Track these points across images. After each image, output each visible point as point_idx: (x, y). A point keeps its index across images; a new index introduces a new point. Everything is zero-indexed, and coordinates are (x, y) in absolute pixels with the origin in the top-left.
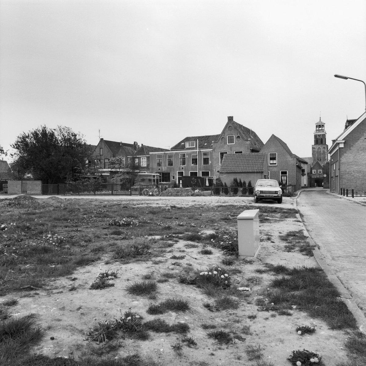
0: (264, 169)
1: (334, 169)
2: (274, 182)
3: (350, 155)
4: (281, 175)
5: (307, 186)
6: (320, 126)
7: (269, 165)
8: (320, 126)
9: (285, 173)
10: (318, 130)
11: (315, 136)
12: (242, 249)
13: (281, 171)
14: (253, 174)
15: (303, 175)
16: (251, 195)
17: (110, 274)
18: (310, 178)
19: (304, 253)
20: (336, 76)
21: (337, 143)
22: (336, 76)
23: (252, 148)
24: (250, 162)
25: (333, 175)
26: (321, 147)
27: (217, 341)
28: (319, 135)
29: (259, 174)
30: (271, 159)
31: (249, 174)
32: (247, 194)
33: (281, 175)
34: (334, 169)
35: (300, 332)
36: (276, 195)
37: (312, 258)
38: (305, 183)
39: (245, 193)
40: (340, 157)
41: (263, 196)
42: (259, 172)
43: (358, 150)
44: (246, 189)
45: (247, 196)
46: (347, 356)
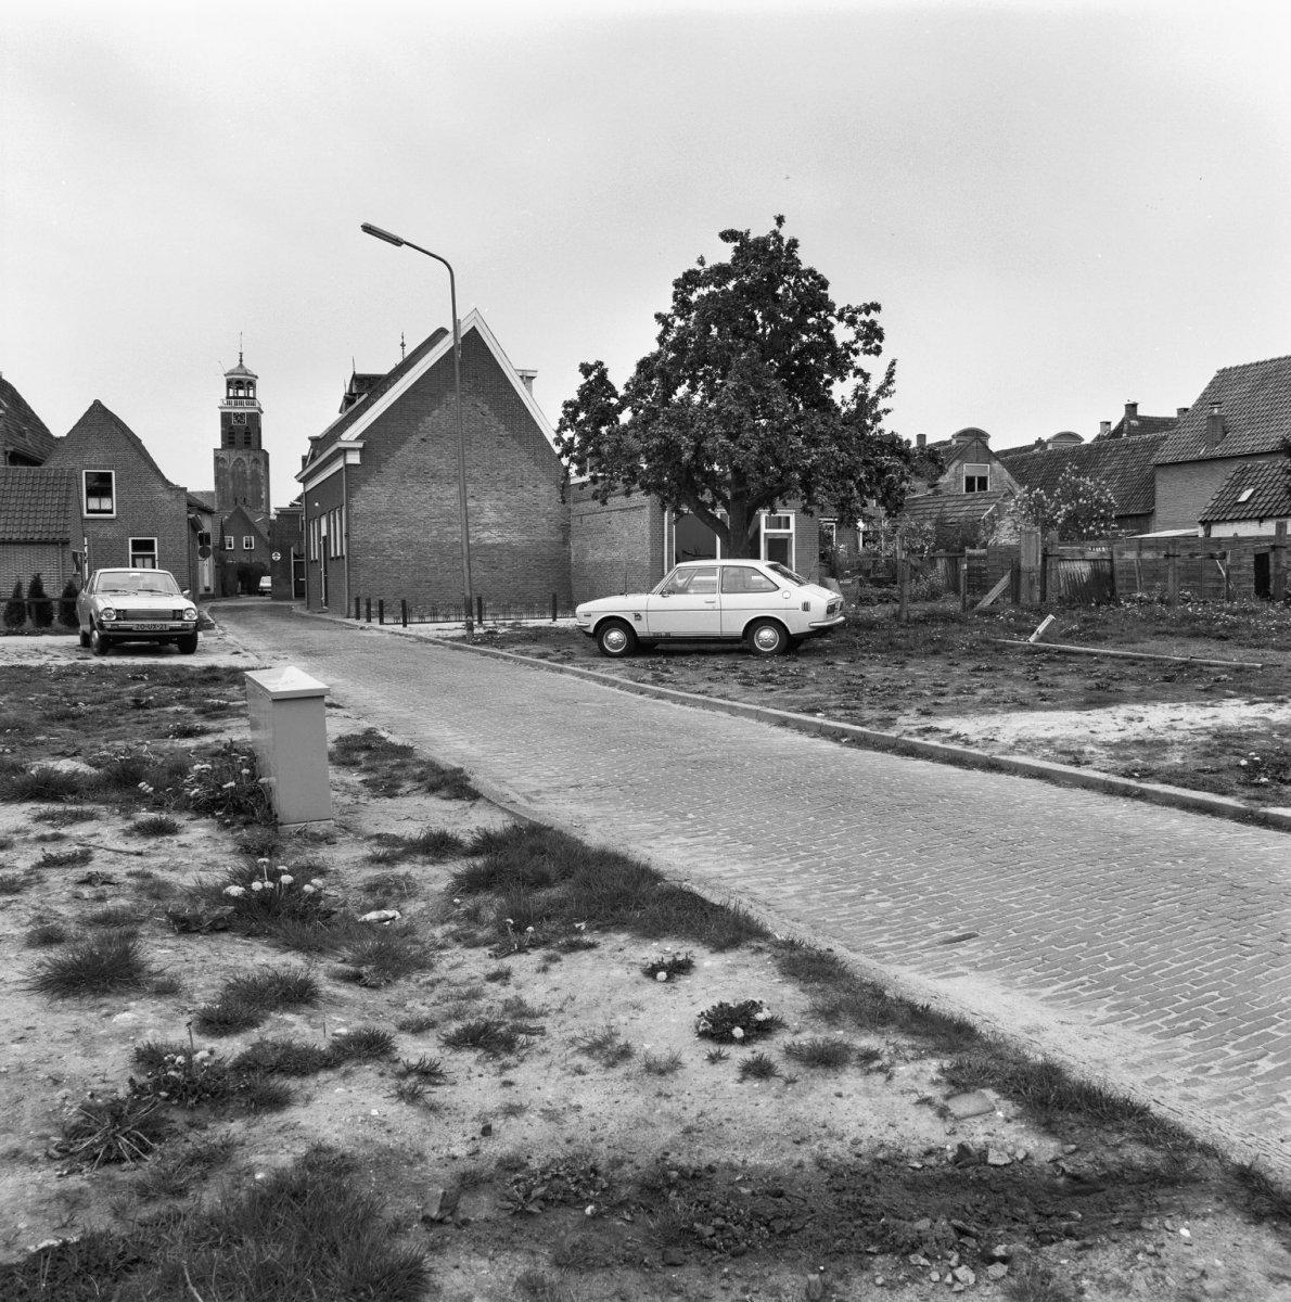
0: (72, 532)
1: (324, 533)
2: (161, 577)
3: (379, 489)
4: (131, 553)
5: (212, 591)
6: (239, 384)
7: (86, 515)
8: (241, 383)
9: (149, 545)
10: (234, 398)
11: (225, 418)
12: (289, 800)
13: (130, 539)
14: (28, 549)
15: (205, 554)
16: (44, 628)
17: (467, 840)
18: (221, 568)
19: (444, 793)
20: (368, 229)
21: (339, 449)
22: (368, 229)
23: (10, 448)
24: (13, 501)
25: (315, 554)
26: (245, 456)
27: (480, 1052)
28: (239, 416)
29: (51, 550)
30: (91, 493)
31: (11, 549)
32: (29, 623)
33: (131, 553)
34: (324, 533)
35: (662, 975)
36: (177, 624)
37: (479, 803)
38: (207, 584)
39: (20, 621)
40: (350, 495)
41: (130, 630)
42: (54, 543)
43: (402, 475)
44: (23, 606)
45: (29, 634)
46: (803, 991)
